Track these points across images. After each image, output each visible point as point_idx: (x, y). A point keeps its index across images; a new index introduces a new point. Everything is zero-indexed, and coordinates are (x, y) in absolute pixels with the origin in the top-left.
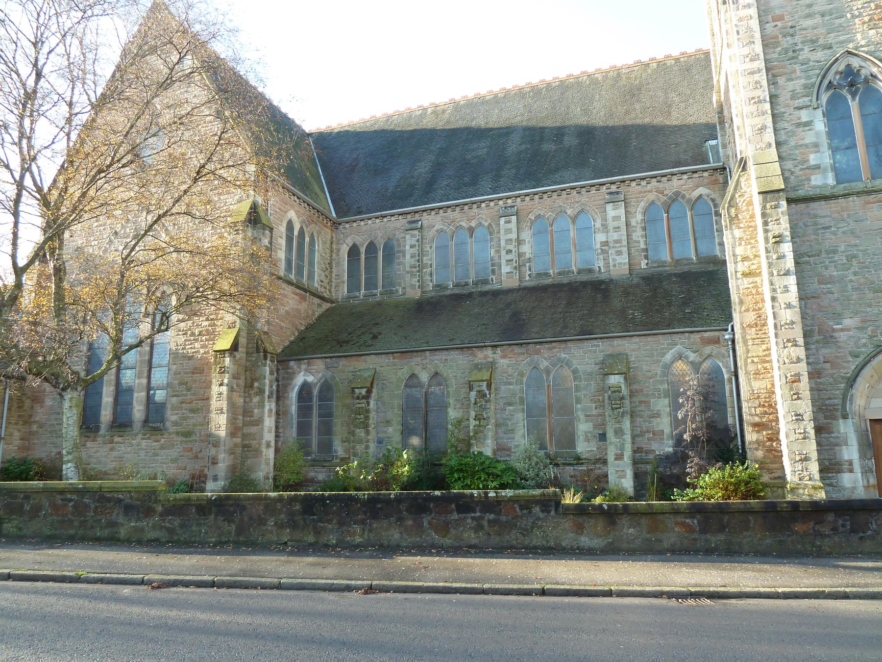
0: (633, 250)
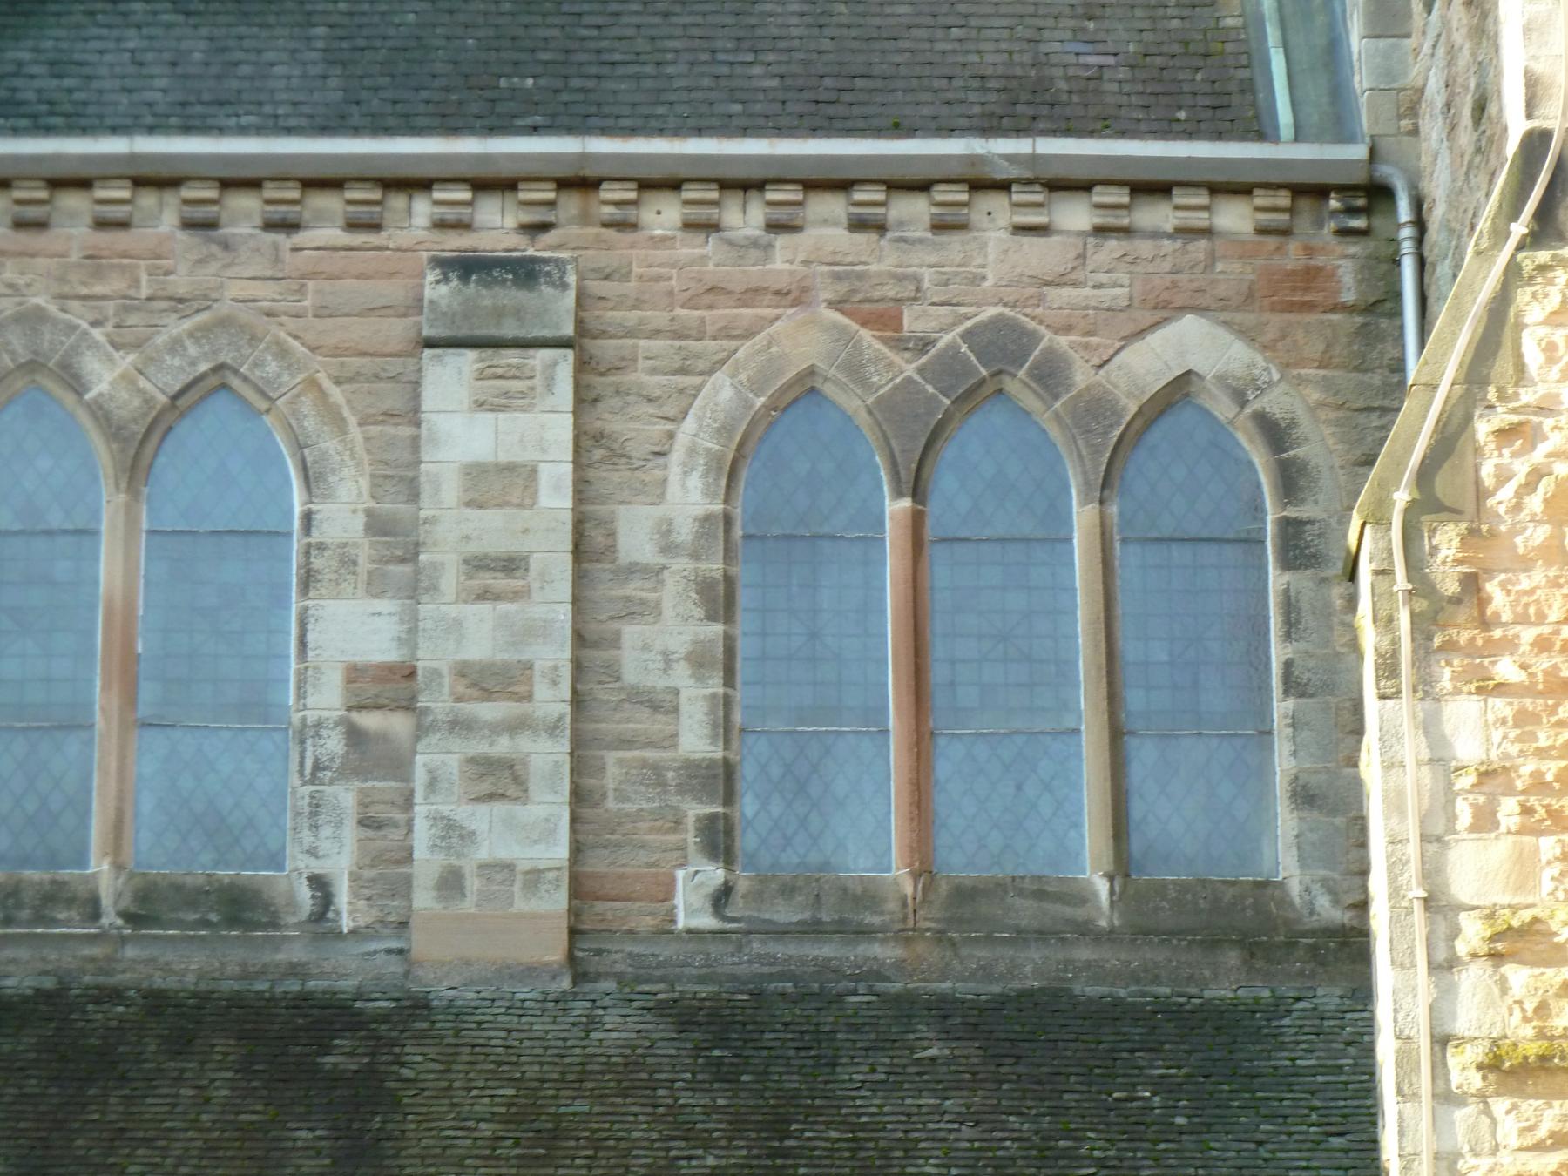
0: (613, 767)
